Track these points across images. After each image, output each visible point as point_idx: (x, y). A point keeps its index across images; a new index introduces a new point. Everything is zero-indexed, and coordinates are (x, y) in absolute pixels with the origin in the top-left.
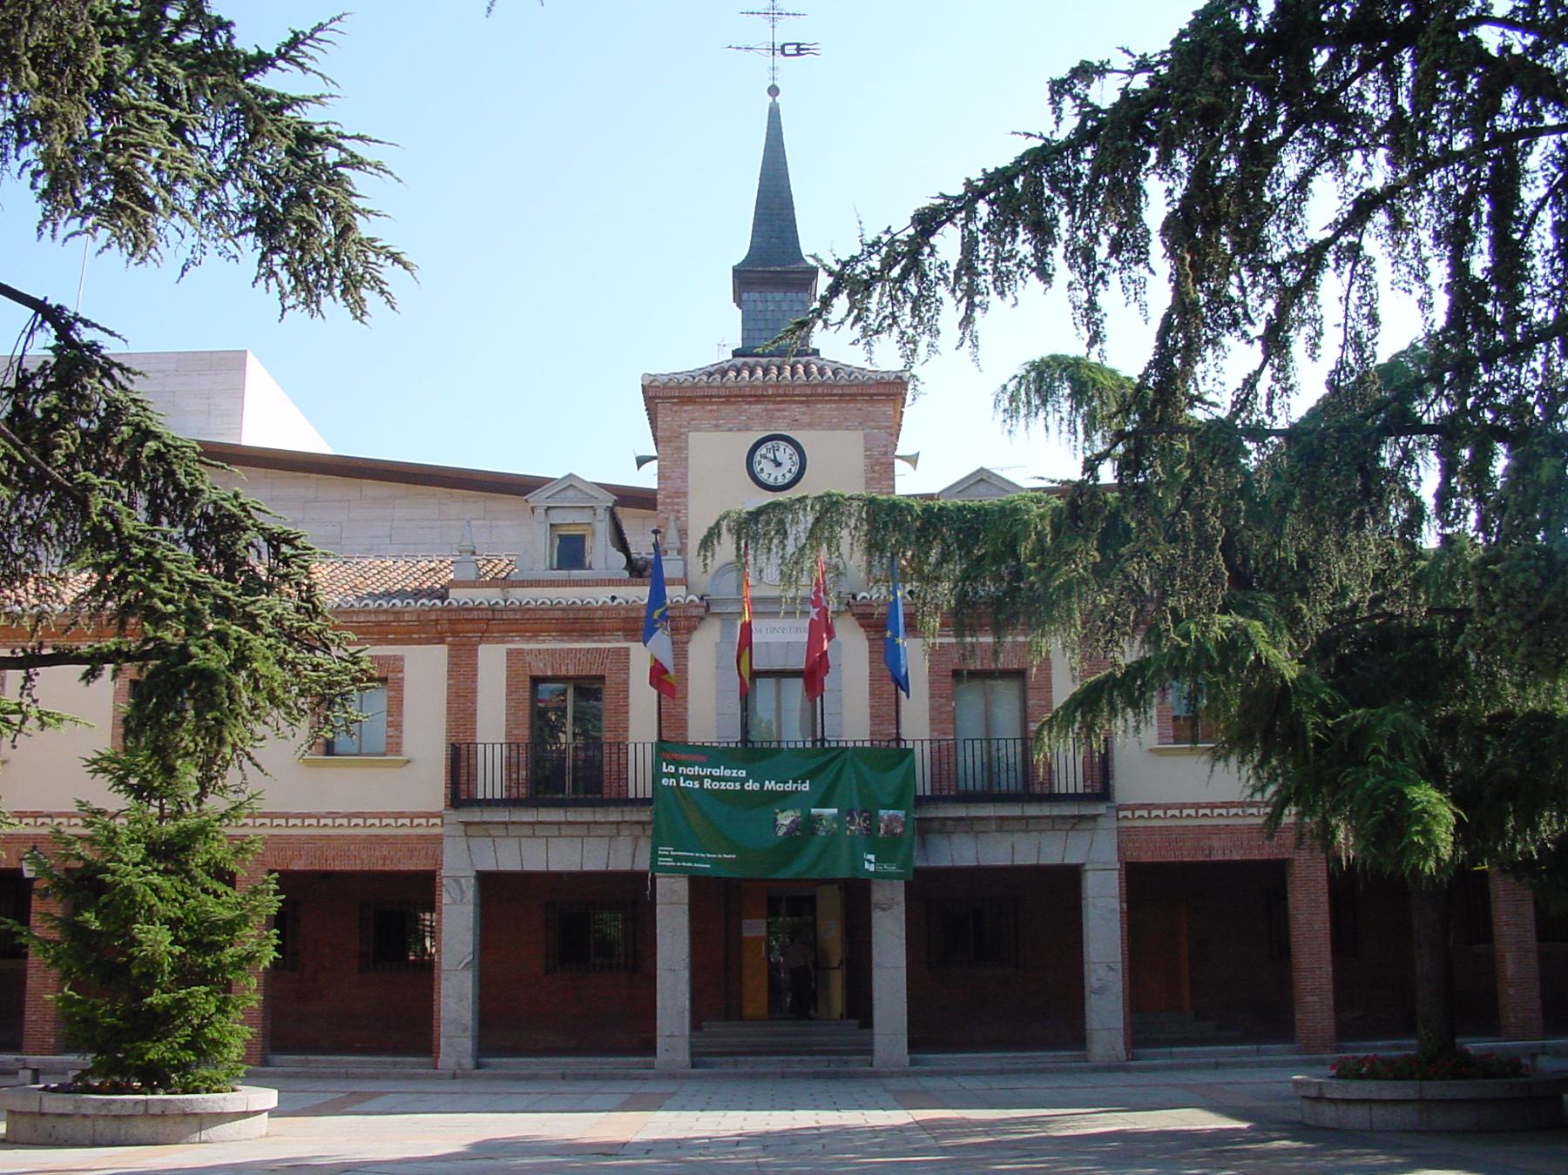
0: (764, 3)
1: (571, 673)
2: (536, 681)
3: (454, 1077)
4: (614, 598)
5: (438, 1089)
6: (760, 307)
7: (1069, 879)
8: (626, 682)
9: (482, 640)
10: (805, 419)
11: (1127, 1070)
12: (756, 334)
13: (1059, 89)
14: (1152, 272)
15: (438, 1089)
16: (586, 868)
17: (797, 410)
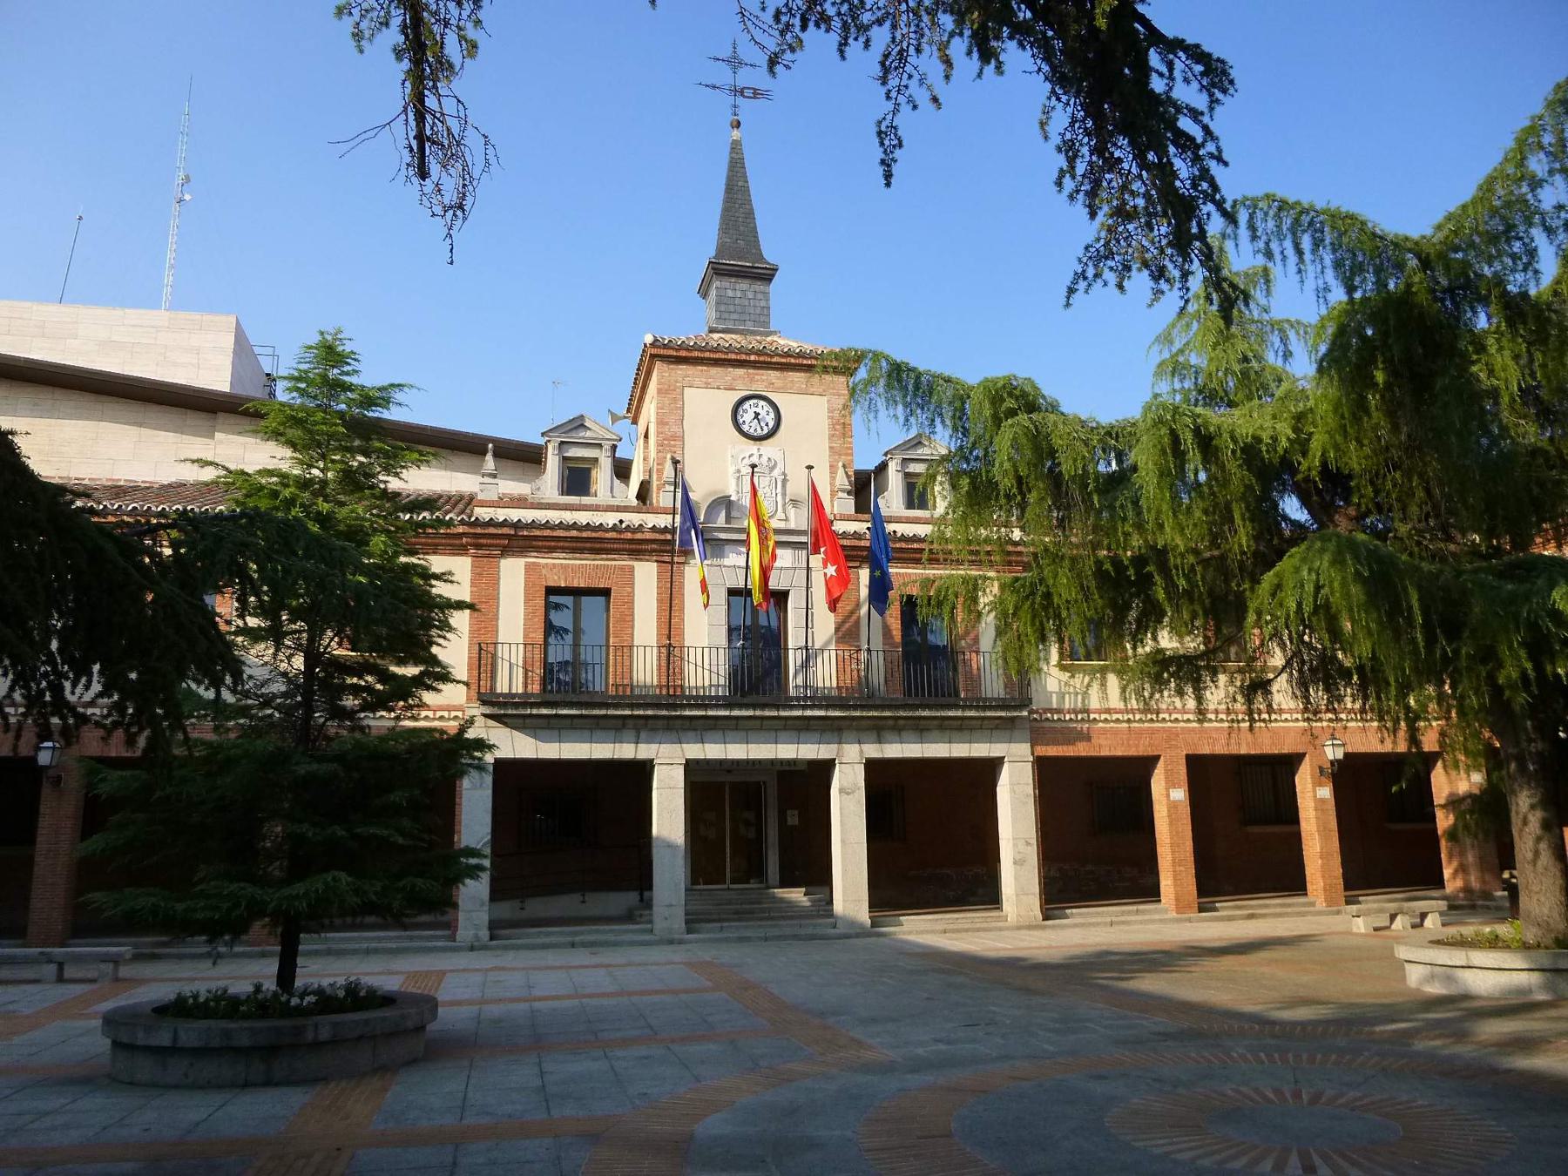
0: (726, 53)
2: (551, 591)
3: (472, 949)
5: (605, 1001)
7: (691, 767)
8: (631, 595)
9: (502, 556)
10: (779, 383)
11: (1044, 927)
12: (726, 315)
13: (543, 434)
14: (1086, 292)
15: (605, 1001)
17: (773, 375)
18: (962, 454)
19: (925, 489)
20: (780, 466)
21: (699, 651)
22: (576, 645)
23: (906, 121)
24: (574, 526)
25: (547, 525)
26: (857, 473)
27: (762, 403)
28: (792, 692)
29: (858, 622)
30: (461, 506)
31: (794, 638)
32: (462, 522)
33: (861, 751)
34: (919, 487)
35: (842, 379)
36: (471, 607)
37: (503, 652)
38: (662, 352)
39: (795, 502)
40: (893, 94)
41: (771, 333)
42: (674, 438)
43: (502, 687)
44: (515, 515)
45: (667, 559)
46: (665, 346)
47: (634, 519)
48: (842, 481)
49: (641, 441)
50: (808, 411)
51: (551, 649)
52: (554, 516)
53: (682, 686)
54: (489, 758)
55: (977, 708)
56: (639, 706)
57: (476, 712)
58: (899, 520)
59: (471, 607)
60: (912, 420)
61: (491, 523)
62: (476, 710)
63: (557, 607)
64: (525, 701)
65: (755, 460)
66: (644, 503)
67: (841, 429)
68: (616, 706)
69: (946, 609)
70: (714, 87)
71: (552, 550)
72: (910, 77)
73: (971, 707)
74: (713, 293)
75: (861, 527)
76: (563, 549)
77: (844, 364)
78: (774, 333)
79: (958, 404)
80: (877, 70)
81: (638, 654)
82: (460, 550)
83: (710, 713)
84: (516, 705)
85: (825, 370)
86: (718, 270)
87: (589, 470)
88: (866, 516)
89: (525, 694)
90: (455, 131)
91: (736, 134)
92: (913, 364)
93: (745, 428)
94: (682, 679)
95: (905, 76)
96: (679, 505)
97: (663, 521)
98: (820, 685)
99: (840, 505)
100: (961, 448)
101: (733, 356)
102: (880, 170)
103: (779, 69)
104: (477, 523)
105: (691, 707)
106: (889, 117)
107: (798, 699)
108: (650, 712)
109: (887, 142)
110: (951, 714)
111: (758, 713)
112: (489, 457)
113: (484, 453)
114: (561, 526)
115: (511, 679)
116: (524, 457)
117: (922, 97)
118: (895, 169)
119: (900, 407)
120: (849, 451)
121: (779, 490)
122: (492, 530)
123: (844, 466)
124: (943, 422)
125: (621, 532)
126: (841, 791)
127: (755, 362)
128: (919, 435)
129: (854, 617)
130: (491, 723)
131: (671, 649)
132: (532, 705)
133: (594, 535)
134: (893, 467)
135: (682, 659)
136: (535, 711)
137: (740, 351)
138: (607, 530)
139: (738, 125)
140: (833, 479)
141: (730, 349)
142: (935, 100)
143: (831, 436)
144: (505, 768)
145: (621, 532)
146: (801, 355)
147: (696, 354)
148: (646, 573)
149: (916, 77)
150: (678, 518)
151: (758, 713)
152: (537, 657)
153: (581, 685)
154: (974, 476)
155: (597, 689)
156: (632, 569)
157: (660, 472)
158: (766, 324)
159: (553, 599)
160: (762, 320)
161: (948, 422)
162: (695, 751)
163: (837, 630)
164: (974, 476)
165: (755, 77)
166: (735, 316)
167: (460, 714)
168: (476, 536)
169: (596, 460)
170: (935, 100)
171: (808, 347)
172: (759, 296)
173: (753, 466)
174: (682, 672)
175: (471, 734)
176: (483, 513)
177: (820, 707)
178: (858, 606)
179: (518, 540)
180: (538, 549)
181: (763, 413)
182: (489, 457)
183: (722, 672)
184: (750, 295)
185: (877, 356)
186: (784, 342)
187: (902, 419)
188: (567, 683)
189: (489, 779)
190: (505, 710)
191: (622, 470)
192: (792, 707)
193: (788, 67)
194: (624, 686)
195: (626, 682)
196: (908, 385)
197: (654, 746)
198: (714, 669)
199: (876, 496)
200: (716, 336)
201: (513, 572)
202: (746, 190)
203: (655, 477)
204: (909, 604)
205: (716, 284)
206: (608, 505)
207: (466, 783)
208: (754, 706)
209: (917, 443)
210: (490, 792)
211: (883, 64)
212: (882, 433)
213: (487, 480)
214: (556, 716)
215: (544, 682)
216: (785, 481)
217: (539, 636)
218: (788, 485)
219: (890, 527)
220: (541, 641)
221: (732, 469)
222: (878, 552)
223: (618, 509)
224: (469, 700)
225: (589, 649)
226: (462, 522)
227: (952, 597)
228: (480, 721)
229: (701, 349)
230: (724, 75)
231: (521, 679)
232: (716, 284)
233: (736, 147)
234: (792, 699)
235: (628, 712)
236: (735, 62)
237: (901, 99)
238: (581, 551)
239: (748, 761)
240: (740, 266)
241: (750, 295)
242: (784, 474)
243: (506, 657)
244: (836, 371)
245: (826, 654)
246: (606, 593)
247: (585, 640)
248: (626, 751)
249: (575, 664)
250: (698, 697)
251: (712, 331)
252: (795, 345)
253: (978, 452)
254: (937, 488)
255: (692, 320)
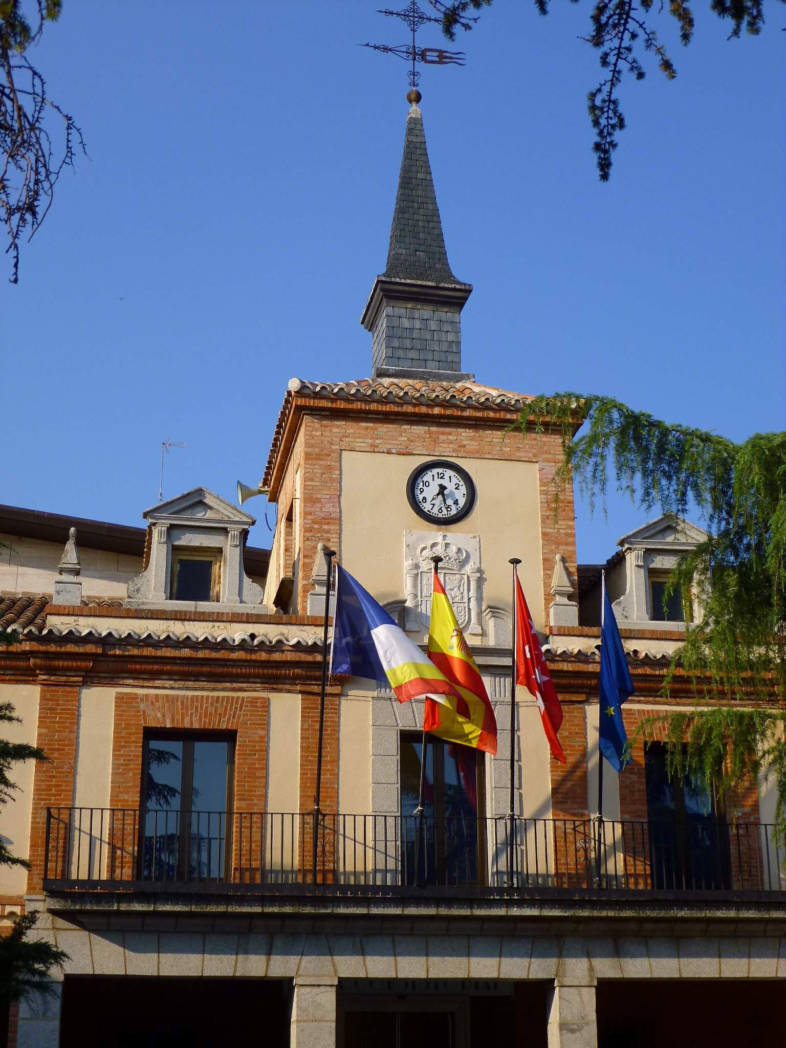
0: (403, 4)
1: (196, 726)
2: (151, 734)
4: (253, 636)
6: (406, 323)
7: (349, 991)
10: (472, 445)
13: (146, 515)
16: (207, 973)
17: (465, 435)
18: (730, 540)
19: (677, 589)
20: (474, 559)
21: (360, 820)
22: (186, 811)
23: (628, 93)
24: (188, 642)
25: (149, 641)
26: (581, 569)
27: (449, 473)
28: (491, 881)
29: (584, 778)
30: (29, 613)
31: (494, 803)
32: (30, 637)
33: (591, 969)
34: (669, 589)
35: (558, 439)
36: (37, 754)
37: (81, 821)
38: (312, 403)
39: (494, 610)
40: (612, 59)
41: (459, 379)
42: (328, 520)
43: (79, 870)
44: (103, 626)
45: (317, 689)
46: (317, 395)
47: (270, 633)
48: (560, 579)
49: (283, 525)
50: (512, 484)
51: (150, 818)
52: (158, 628)
53: (335, 872)
54: (56, 973)
55: (758, 905)
56: (273, 900)
57: (40, 907)
58: (641, 635)
59: (37, 754)
60: (654, 493)
61: (71, 637)
62: (41, 904)
63: (162, 756)
64: (109, 891)
65: (439, 551)
66: (286, 611)
67: (557, 507)
68: (241, 900)
69: (709, 759)
70: (386, 49)
71: (154, 675)
72: (634, 36)
73: (748, 905)
74: (383, 323)
75: (588, 644)
76: (170, 675)
77: (555, 419)
78: (467, 377)
79: (719, 470)
80: (590, 29)
81: (274, 826)
82: (24, 675)
83: (375, 911)
84: (98, 898)
85: (530, 427)
86: (388, 292)
87: (209, 565)
88: (595, 630)
89: (111, 881)
90: (29, 110)
91: (415, 110)
92: (656, 417)
93: (427, 507)
94: (336, 862)
95: (627, 35)
96: (333, 613)
97: (311, 635)
98: (532, 870)
99: (555, 614)
100: (726, 533)
101: (410, 409)
102: (594, 158)
103: (457, 29)
104: (51, 638)
105: (347, 901)
106: (606, 88)
107: (500, 890)
108: (288, 910)
109: (603, 121)
110: (720, 914)
111: (443, 911)
112: (70, 546)
113: (63, 540)
114: (168, 642)
115: (90, 861)
116: (119, 546)
117: (649, 61)
118: (614, 156)
119: (638, 475)
120: (569, 539)
121: (473, 593)
122: (70, 648)
123: (563, 560)
124: (698, 496)
125: (252, 650)
126: (563, 1026)
127: (440, 416)
128: (666, 517)
129: (578, 773)
130: (61, 923)
131: (320, 818)
132: (120, 898)
133: (214, 655)
134: (632, 560)
135: (335, 832)
136: (124, 907)
137: (418, 402)
138: (233, 649)
139: (418, 98)
140: (548, 577)
141: (405, 399)
142: (667, 65)
143: (544, 519)
144: (80, 988)
145: (252, 650)
146: (503, 407)
147: (358, 405)
148: (286, 710)
149: (642, 36)
150: (332, 631)
151: (443, 911)
152: (129, 829)
153: (192, 870)
154: (743, 570)
155: (214, 875)
156: (266, 704)
157: (308, 567)
158: (455, 365)
159: (154, 745)
160: (450, 362)
161: (707, 496)
162: (352, 966)
163: (555, 791)
164: (743, 570)
165: (431, 36)
166: (412, 354)
167: (17, 909)
168: (47, 655)
169: (220, 551)
170: (667, 65)
171: (512, 396)
172: (446, 327)
173: (437, 560)
174: (335, 852)
175: (31, 937)
176: (59, 624)
177: (531, 904)
178: (584, 756)
179: (107, 661)
180: (136, 675)
181: (450, 487)
182: (70, 546)
183: (391, 851)
184: (433, 326)
185: (607, 405)
186: (478, 390)
187: (639, 493)
188: (171, 867)
189: (56, 1005)
190: (82, 905)
191: (255, 565)
192: (491, 904)
193: (467, 27)
194: (252, 870)
195: (255, 864)
196: (652, 447)
197: (293, 960)
198: (360, 838)
199: (610, 600)
200: (386, 381)
201: (98, 707)
202: (428, 184)
203: (301, 575)
204: (656, 750)
205: (387, 310)
206: (236, 613)
207: (23, 1009)
208: (437, 902)
209: (667, 526)
210: (56, 1023)
211: (596, 19)
212: (615, 512)
213: (66, 577)
214: (155, 913)
215: (140, 863)
216: (480, 581)
217: (133, 798)
218: (486, 587)
219: (630, 646)
220: (136, 805)
221: (407, 564)
222: (618, 676)
223: (248, 619)
224: (31, 888)
225: (204, 817)
226: (30, 637)
227: (716, 742)
228: (44, 920)
229: (366, 399)
230: (398, 33)
231: (105, 861)
232: (387, 310)
233: (415, 127)
234: (492, 890)
235: (257, 909)
236: (414, 17)
237: (623, 65)
238: (197, 677)
239: (428, 982)
240: (419, 285)
241: (433, 326)
242: (479, 570)
243: (86, 827)
244: (549, 428)
245: (540, 824)
246: (229, 736)
247: (199, 804)
248: (253, 966)
249: (184, 840)
250: (357, 887)
251: (381, 374)
252: (494, 393)
253: (750, 539)
254: (695, 590)
255: (354, 361)
